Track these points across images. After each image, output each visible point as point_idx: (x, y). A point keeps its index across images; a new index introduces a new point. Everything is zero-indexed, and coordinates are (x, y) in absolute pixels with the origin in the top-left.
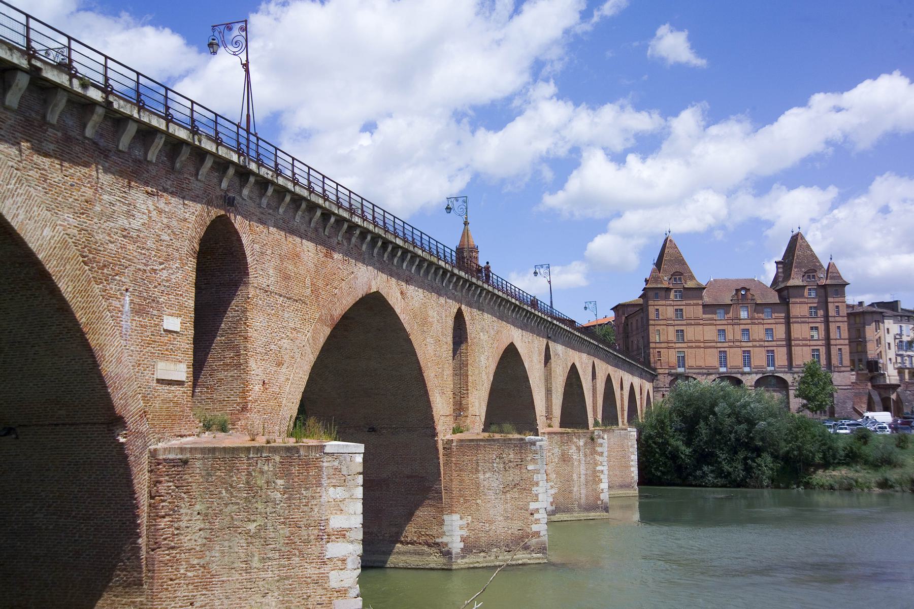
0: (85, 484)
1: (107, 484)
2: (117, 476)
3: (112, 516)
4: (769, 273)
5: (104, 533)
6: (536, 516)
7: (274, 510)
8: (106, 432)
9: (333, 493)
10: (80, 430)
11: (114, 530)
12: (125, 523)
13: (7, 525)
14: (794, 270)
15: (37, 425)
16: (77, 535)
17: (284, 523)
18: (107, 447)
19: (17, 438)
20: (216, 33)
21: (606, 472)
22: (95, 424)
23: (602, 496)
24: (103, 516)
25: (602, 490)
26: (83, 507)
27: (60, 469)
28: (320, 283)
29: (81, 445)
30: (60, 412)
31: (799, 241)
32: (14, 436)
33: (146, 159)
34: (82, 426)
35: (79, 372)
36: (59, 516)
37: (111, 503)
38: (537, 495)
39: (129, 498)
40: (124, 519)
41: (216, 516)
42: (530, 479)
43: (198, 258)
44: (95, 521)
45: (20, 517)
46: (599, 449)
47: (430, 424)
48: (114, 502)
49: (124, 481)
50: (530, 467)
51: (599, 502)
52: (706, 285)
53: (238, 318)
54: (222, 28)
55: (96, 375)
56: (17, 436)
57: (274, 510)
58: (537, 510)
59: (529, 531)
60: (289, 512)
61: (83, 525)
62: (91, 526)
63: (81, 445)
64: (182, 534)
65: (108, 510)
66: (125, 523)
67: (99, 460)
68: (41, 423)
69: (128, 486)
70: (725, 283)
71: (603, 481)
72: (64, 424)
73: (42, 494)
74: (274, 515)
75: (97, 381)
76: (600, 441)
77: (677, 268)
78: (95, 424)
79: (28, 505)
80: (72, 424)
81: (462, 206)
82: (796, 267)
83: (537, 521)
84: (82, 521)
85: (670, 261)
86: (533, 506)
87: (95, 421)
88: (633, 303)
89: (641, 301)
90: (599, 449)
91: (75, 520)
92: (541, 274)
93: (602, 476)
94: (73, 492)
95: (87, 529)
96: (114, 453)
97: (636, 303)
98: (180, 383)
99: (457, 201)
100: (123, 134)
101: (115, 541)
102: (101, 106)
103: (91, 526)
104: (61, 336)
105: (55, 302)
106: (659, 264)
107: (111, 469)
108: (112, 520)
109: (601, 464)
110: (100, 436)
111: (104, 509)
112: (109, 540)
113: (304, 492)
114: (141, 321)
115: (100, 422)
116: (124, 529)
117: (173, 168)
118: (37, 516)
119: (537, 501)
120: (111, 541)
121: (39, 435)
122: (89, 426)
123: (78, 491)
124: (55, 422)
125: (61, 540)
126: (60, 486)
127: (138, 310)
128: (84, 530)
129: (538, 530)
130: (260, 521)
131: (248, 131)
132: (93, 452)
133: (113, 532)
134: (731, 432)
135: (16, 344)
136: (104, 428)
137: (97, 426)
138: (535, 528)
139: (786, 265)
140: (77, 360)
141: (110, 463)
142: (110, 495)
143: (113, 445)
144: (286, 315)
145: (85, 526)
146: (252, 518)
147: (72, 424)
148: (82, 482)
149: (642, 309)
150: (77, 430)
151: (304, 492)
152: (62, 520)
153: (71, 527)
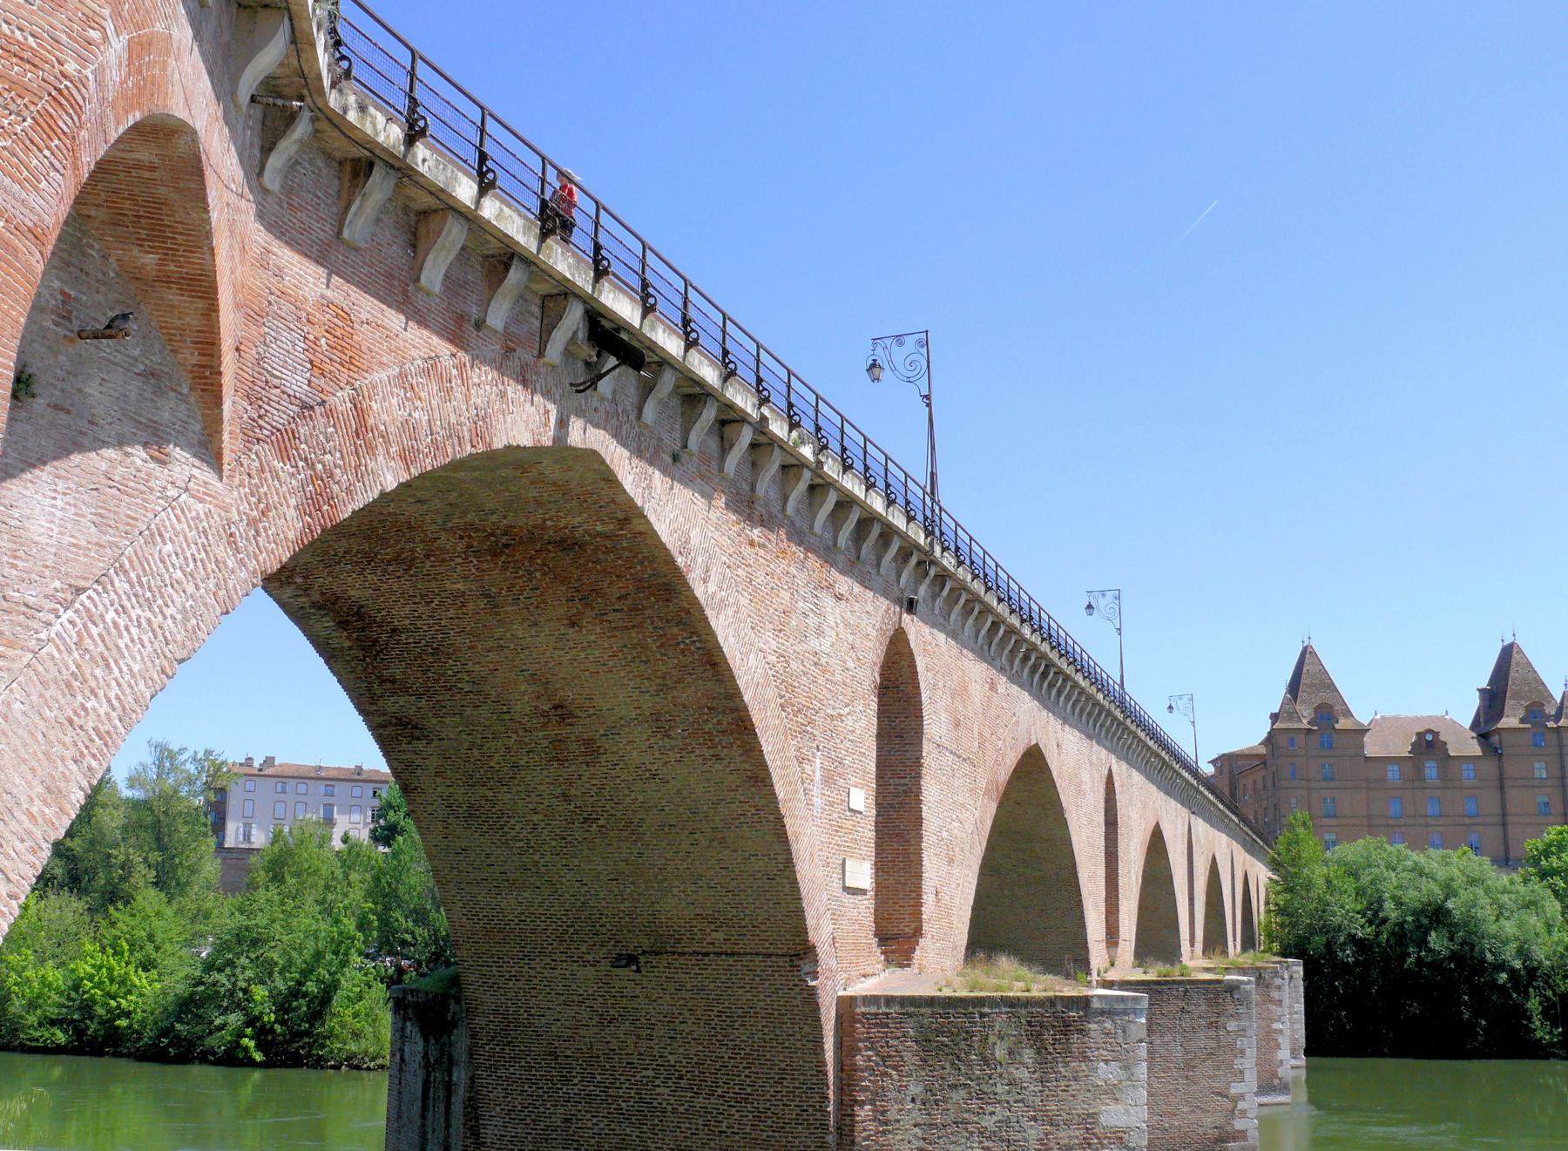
0: (743, 1047)
1: (780, 1050)
2: (798, 1037)
3: (785, 1099)
4: (1463, 709)
5: (769, 1123)
6: (1241, 1105)
7: (1020, 1097)
8: (788, 969)
9: (1107, 1072)
10: (745, 963)
11: (787, 1121)
12: (806, 1111)
13: (610, 1101)
14: (1509, 703)
15: (673, 953)
16: (724, 1124)
17: (1034, 1119)
18: (786, 991)
19: (638, 970)
20: (879, 350)
21: (1287, 1032)
22: (770, 955)
23: (1280, 1072)
24: (768, 1097)
25: (1281, 1061)
26: (737, 1082)
27: (702, 1022)
28: (987, 734)
29: (742, 987)
30: (715, 935)
31: (1516, 656)
32: (634, 968)
33: (835, 544)
34: (749, 957)
35: (759, 875)
36: (695, 1093)
37: (784, 1079)
38: (1241, 1072)
39: (814, 1073)
40: (805, 1104)
41: (937, 1105)
42: (1232, 1047)
43: (881, 696)
44: (755, 1105)
45: (633, 1091)
46: (1275, 995)
47: (1080, 955)
48: (789, 1077)
49: (810, 1045)
50: (1232, 1026)
51: (1276, 1082)
52: (1369, 725)
53: (905, 788)
54: (888, 342)
55: (785, 881)
56: (638, 967)
57: (1020, 1097)
58: (1242, 1097)
59: (1229, 1129)
60: (1042, 1101)
61: (734, 1109)
62: (749, 1112)
63: (742, 987)
64: (890, 1132)
65: (779, 1089)
66: (806, 1111)
67: (770, 1011)
68: (680, 950)
69: (815, 1054)
70: (1397, 722)
71: (1282, 1046)
72: (718, 954)
73: (670, 1057)
74: (1020, 1105)
75: (787, 891)
76: (1278, 981)
77: (1324, 696)
78: (770, 955)
79: (645, 1073)
80: (733, 954)
81: (1111, 605)
82: (1512, 698)
83: (1243, 1113)
84: (733, 1104)
85: (1311, 686)
86: (1235, 1089)
87: (772, 950)
88: (1247, 752)
89: (1263, 750)
90: (1275, 995)
91: (721, 1102)
92: (1178, 710)
93: (1280, 1040)
94: (723, 1057)
95: (741, 1116)
96: (796, 1002)
97: (1255, 752)
98: (863, 892)
99: (1104, 595)
100: (820, 507)
101: (786, 1137)
102: (810, 470)
103: (749, 1112)
104: (742, 820)
105: (747, 767)
106: (1294, 687)
107: (789, 1025)
108: (783, 1105)
109: (1279, 1020)
110: (777, 974)
111: (771, 1086)
112: (777, 1134)
113: (1063, 1070)
114: (829, 796)
115: (780, 952)
116: (804, 1120)
117: (858, 558)
118: (658, 1090)
119: (1242, 1080)
120: (780, 1136)
121: (675, 968)
122: (760, 958)
123: (730, 1058)
124: (704, 950)
125: (697, 1129)
126: (700, 1048)
127: (828, 780)
128: (737, 1117)
129: (1243, 1128)
130: (1001, 1113)
131: (933, 500)
132: (762, 997)
133: (784, 1123)
134: (298, 875)
135: (666, 829)
136: (784, 962)
137: (773, 958)
138: (1239, 1124)
139: (1494, 699)
140: (760, 857)
141: (789, 1016)
142: (783, 1065)
143: (797, 989)
144: (956, 784)
145: (738, 1111)
146: (990, 1108)
147: (733, 954)
148: (737, 1043)
149: (1264, 763)
150: (739, 963)
151: (1063, 1070)
152: (701, 1100)
153: (715, 1111)
